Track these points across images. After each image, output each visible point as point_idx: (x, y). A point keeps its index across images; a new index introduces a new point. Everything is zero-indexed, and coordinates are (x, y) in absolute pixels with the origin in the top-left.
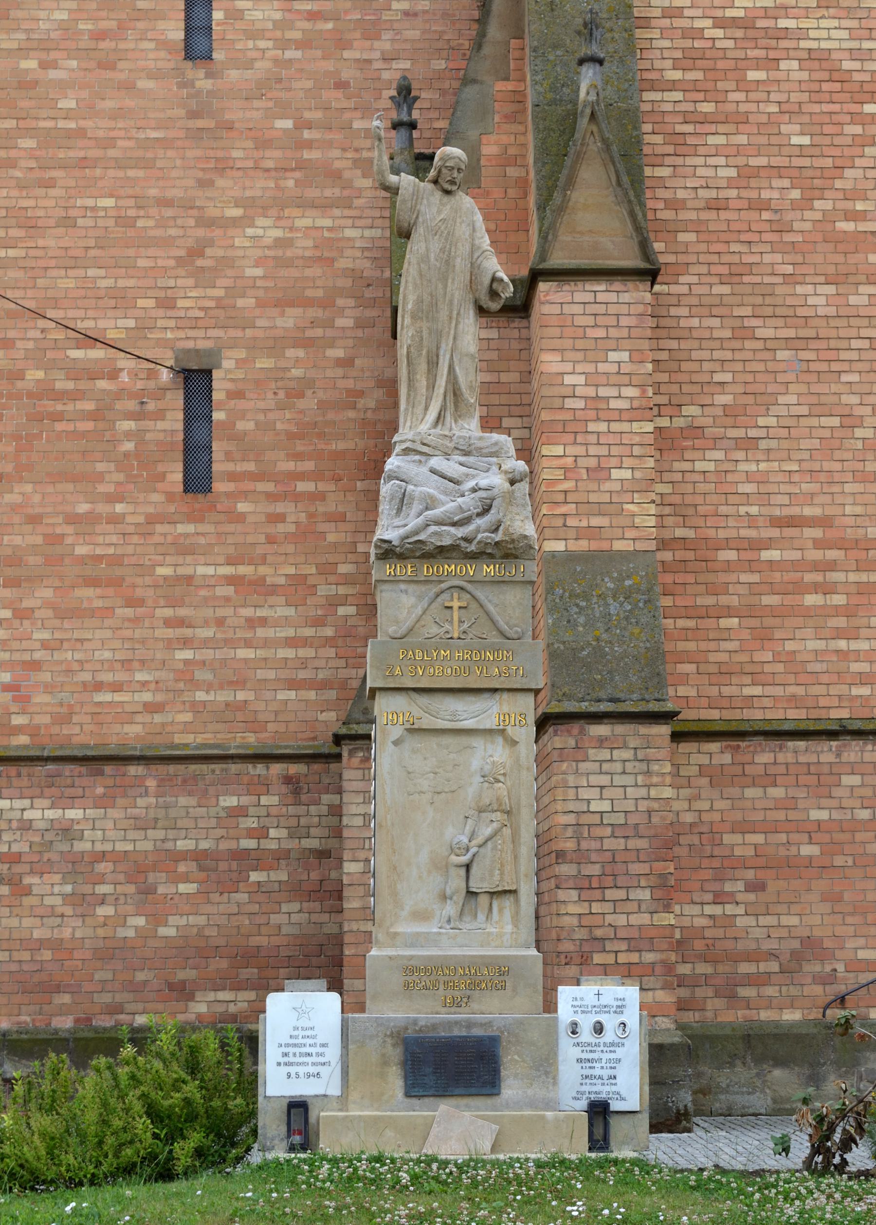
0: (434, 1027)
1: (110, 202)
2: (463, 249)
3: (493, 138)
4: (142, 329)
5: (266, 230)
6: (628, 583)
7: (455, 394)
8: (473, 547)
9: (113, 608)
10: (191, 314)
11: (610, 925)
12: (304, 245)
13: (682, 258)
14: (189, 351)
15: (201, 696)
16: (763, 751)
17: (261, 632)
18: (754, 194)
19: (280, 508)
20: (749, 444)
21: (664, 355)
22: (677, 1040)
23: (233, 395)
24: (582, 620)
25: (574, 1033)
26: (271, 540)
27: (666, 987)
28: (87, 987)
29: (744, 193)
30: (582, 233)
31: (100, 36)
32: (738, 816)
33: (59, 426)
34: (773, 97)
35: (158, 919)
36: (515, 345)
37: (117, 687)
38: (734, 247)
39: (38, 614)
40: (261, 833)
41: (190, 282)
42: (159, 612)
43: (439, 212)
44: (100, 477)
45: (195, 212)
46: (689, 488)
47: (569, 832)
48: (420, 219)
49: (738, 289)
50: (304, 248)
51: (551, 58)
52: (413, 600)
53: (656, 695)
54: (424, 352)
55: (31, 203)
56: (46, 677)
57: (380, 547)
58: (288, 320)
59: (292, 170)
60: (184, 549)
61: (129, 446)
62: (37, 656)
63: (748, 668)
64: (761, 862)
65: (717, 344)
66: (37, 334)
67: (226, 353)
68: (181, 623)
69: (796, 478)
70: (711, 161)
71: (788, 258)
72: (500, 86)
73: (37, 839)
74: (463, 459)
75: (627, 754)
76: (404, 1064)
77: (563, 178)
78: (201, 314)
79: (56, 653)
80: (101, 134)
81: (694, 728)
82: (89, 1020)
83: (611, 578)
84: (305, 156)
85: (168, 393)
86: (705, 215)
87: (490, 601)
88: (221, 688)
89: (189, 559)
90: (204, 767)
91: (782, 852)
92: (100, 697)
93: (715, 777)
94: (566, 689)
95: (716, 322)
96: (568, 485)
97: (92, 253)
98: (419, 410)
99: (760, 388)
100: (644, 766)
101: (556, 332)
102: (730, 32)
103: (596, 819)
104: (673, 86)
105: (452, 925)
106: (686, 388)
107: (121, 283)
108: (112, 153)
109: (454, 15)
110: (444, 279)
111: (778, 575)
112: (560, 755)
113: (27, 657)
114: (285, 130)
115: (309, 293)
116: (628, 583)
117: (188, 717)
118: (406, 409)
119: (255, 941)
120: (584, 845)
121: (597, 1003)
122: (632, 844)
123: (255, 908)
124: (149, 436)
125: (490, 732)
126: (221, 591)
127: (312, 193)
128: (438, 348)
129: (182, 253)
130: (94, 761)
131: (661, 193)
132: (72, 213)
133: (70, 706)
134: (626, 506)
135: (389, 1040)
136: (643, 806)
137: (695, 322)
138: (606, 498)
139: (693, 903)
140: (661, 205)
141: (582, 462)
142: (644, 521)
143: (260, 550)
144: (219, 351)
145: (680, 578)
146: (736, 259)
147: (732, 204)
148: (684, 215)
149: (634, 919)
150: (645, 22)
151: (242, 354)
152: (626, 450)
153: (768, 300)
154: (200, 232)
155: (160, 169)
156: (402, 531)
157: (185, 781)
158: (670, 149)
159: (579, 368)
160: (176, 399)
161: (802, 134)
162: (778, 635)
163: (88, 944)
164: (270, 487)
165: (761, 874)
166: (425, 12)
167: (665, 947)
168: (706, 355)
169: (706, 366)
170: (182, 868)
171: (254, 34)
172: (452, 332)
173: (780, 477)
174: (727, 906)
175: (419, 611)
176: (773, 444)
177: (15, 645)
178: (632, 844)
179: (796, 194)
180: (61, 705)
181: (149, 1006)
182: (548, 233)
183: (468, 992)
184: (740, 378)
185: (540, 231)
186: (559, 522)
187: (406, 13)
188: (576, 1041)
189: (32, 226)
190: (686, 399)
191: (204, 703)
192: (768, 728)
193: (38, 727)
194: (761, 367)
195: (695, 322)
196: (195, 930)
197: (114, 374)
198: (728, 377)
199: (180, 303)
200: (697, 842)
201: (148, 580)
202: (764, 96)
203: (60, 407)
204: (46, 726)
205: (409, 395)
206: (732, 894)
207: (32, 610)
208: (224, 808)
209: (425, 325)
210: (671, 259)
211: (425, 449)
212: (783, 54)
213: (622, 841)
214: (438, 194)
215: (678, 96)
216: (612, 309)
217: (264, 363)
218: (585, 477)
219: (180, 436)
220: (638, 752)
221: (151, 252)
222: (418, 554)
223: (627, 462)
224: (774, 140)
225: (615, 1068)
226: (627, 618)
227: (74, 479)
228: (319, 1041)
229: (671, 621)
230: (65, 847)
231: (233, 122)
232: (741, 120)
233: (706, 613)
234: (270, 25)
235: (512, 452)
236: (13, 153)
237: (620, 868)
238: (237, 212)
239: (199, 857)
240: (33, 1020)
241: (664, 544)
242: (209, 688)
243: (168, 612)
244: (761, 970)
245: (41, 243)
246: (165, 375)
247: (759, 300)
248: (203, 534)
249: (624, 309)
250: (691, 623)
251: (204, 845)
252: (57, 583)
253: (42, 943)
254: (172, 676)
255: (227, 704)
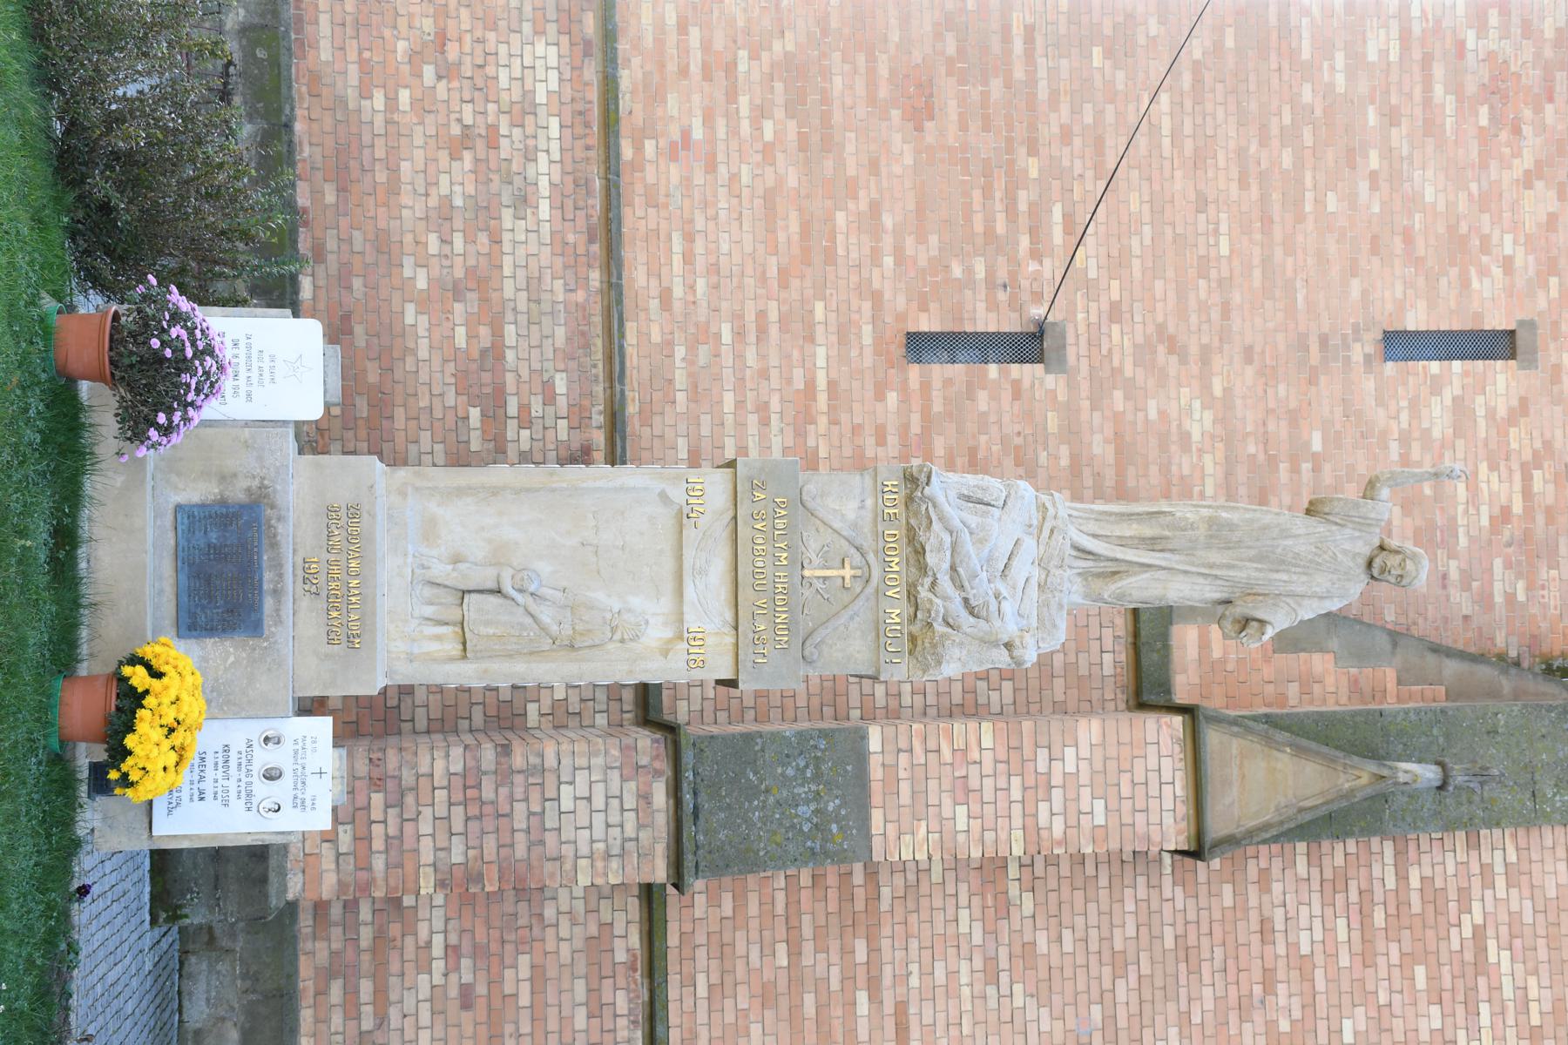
0: (274, 545)
1: (1224, 250)
2: (1299, 584)
3: (1331, 666)
4: (1090, 287)
5: (1200, 423)
6: (834, 827)
7: (1115, 573)
8: (924, 593)
9: (776, 254)
10: (1104, 340)
11: (419, 813)
12: (1183, 464)
13: (1203, 889)
14: (1064, 338)
15: (680, 352)
16: (630, 1001)
17: (753, 419)
18: (1281, 975)
19: (893, 440)
20: (991, 974)
21: (1090, 870)
22: (274, 902)
23: (1016, 386)
24: (790, 772)
25: (267, 740)
26: (856, 429)
27: (342, 885)
28: (344, 222)
29: (1281, 963)
30: (1241, 767)
31: (1408, 238)
32: (552, 972)
33: (977, 195)
34: (1397, 997)
35: (424, 305)
36: (1096, 695)
37: (688, 258)
38: (1218, 952)
39: (769, 170)
40: (525, 421)
41: (1140, 339)
42: (773, 305)
43: (1345, 552)
44: (921, 239)
45: (1216, 343)
46: (938, 903)
47: (534, 760)
48: (1334, 528)
49: (1171, 957)
50: (1180, 465)
51: (1435, 731)
52: (851, 516)
53: (702, 864)
54: (1167, 533)
55: (1221, 164)
56: (699, 178)
57: (921, 471)
58: (1100, 447)
59: (1266, 452)
60: (844, 334)
61: (957, 271)
62: (722, 169)
63: (728, 979)
64: (497, 1003)
65: (1105, 934)
66: (1077, 170)
67: (1062, 378)
68: (762, 331)
69: (954, 1031)
70: (1317, 923)
71: (1209, 1017)
72: (1390, 675)
73: (515, 168)
74: (1034, 582)
75: (630, 830)
76: (223, 502)
77: (1304, 742)
78: (1104, 352)
79: (725, 190)
80: (1300, 239)
81: (656, 917)
82: (306, 224)
83: (840, 807)
84: (1282, 466)
85: (1016, 315)
86: (1254, 916)
87: (852, 618)
88: (690, 375)
89: (834, 338)
90: (600, 356)
91: (509, 1029)
92: (677, 238)
93: (598, 945)
94: (708, 753)
95: (1131, 931)
96: (947, 754)
97: (1168, 230)
98: (1092, 527)
99: (1056, 987)
100: (616, 851)
101: (1125, 738)
102: (1469, 944)
103: (550, 793)
104: (1402, 877)
105: (418, 571)
106: (1053, 896)
107: (1136, 263)
108: (1279, 252)
109: (1446, 630)
110: (1260, 558)
111: (839, 1013)
112: (628, 747)
113: (721, 157)
114: (1308, 444)
115: (1131, 471)
116: (834, 827)
117: (656, 337)
118: (1092, 511)
119: (399, 413)
120: (518, 779)
121: (308, 771)
122: (520, 838)
123: (438, 414)
124: (968, 293)
125: (680, 620)
126: (798, 375)
127: (1241, 473)
128: (1172, 551)
129: (1171, 330)
130: (610, 236)
131: (1277, 864)
132: (1212, 208)
133: (666, 206)
134: (924, 823)
135: (256, 483)
136: (567, 850)
137: (1130, 907)
138: (933, 800)
139: (447, 920)
140: (1263, 865)
141: (974, 769)
142: (907, 847)
143: (844, 417)
144: (1064, 372)
145: (833, 894)
146: (1206, 954)
147: (1268, 949)
148: (1253, 891)
149: (426, 845)
150: (1473, 844)
151: (1062, 397)
152: (989, 824)
153: (1159, 994)
154: (1194, 350)
155: (1263, 306)
156: (941, 499)
157: (583, 334)
158: (1328, 874)
159: (1084, 765)
160: (1010, 324)
161: (1356, 1033)
162: (769, 1014)
163: (395, 224)
164: (916, 428)
165: (481, 1004)
166: (1448, 598)
167: (392, 882)
168: (914, 953)
169: (1079, 921)
170: (484, 331)
171: (1414, 406)
172: (1194, 569)
173: (953, 1013)
174: (442, 963)
175: (837, 525)
176: (992, 1003)
177: (734, 145)
178: (520, 838)
179: (1284, 1026)
180: (667, 196)
181: (322, 294)
182: (1240, 726)
183: (324, 594)
184: (1068, 960)
185: (1243, 717)
186: (903, 744)
187: (1445, 576)
188: (255, 743)
189: (1198, 162)
190: (1041, 898)
191: (671, 356)
192: (658, 1006)
193: (642, 170)
194: (1081, 987)
195: (1130, 907)
196: (411, 345)
197: (1036, 255)
198: (1068, 946)
199: (1116, 328)
200: (521, 922)
201: (809, 292)
202: (1397, 986)
203: (998, 195)
204: (644, 179)
205: (1111, 514)
206: (458, 968)
207: (773, 164)
208: (552, 377)
209: (1202, 531)
210: (1202, 877)
211: (1046, 533)
212: (1448, 1010)
213: (524, 826)
214: (1366, 551)
215: (1391, 883)
216: (1154, 804)
217: (1053, 422)
218: (957, 774)
219: (969, 329)
220: (633, 843)
221: (1171, 295)
222: (912, 521)
223: (976, 825)
224: (1346, 999)
225: (215, 798)
226: (793, 826)
227: (920, 210)
228: (255, 389)
229: (783, 885)
230: (506, 199)
231: (1317, 385)
232: (1367, 958)
233: (792, 928)
234: (1425, 425)
235: (1046, 647)
236: (1275, 143)
237: (489, 824)
238: (1218, 391)
239: (495, 352)
240: (304, 161)
241: (872, 872)
242: (690, 360)
243: (773, 316)
244: (363, 1008)
245: (1178, 174)
246: (1038, 311)
247: (1159, 983)
248: (861, 354)
249: (1154, 819)
250: (780, 908)
251: (510, 356)
252: (803, 192)
253: (394, 171)
254: (703, 319)
255: (671, 381)
